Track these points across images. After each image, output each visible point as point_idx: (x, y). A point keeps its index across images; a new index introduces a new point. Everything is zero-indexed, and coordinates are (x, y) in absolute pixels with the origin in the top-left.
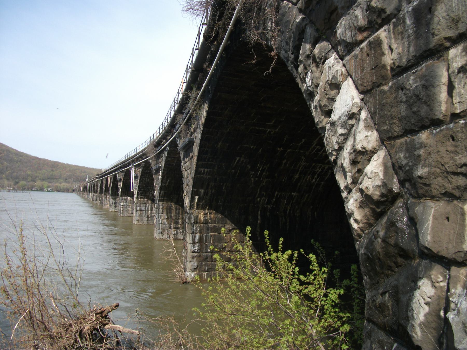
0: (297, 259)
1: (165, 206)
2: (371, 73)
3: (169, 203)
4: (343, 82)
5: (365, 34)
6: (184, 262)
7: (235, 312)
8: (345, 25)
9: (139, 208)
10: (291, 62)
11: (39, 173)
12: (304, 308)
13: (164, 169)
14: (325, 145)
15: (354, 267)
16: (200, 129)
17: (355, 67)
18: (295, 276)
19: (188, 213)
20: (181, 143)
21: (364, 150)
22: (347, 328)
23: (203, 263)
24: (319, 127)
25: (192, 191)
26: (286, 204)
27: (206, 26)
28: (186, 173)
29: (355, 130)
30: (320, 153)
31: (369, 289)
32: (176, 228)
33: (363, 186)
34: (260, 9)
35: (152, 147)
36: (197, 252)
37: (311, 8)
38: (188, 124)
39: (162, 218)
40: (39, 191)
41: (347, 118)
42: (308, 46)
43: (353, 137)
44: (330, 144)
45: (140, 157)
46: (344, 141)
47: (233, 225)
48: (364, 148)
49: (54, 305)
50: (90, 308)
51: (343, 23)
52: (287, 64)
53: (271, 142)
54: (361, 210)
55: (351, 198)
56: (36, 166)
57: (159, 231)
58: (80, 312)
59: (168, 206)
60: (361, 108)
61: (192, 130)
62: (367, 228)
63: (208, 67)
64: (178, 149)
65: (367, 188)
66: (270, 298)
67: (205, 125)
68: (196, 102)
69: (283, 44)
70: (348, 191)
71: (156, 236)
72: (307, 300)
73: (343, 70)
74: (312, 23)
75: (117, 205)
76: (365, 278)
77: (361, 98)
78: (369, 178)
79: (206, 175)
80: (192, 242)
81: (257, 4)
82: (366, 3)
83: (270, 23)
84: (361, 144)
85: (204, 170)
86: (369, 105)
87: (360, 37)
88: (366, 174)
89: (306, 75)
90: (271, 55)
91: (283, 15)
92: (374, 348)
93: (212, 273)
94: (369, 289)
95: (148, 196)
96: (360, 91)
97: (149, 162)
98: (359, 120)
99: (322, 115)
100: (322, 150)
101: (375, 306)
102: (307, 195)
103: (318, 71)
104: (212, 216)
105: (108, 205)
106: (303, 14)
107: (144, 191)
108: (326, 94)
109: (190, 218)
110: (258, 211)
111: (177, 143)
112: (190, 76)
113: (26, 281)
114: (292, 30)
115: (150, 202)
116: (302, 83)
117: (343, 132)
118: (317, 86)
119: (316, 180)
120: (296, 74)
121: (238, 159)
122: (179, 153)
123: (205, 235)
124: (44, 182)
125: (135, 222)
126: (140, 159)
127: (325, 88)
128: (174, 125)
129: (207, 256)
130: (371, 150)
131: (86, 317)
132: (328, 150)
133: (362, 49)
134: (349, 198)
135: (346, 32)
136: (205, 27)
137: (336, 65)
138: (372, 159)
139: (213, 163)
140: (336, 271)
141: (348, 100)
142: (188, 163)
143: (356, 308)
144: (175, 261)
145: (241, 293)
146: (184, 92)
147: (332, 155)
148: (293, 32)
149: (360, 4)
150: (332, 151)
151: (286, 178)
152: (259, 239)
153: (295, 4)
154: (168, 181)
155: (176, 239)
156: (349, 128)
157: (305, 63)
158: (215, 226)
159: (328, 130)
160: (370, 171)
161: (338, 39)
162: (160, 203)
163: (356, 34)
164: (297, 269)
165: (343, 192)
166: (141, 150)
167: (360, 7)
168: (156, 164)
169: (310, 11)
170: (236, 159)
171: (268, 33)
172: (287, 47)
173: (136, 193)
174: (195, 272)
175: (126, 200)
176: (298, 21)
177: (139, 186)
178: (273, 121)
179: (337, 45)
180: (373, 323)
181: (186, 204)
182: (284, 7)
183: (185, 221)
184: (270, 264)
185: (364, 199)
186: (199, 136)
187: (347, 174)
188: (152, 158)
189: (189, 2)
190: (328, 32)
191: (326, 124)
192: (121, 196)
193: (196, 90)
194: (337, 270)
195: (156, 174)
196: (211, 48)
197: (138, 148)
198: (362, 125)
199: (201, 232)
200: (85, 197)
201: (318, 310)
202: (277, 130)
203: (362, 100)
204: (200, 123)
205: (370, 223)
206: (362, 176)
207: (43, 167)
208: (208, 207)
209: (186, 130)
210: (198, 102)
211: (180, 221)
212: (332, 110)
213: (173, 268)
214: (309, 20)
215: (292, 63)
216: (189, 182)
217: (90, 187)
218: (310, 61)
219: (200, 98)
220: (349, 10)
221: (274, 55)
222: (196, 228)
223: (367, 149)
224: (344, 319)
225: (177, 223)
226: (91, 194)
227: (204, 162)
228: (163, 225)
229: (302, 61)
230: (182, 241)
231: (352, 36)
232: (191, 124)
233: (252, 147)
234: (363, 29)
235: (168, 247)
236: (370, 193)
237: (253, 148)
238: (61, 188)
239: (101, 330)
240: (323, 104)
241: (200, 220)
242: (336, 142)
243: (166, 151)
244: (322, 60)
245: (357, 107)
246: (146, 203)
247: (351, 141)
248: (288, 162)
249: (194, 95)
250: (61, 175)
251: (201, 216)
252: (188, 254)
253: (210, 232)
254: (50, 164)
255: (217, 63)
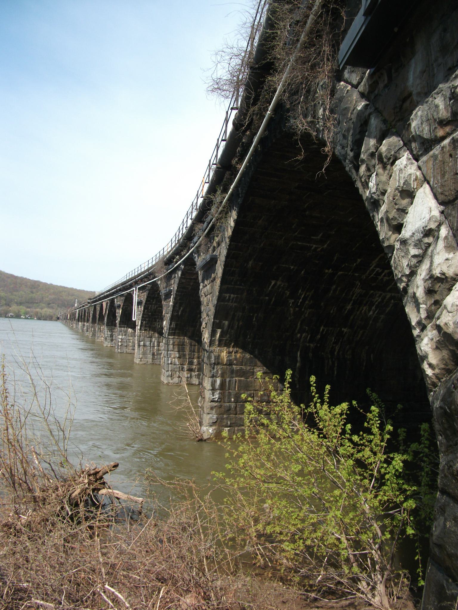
0: (348, 412)
1: (177, 341)
2: (454, 179)
3: (182, 338)
4: (417, 189)
5: (448, 129)
6: (200, 414)
7: (269, 479)
8: (421, 116)
9: (142, 342)
10: (350, 161)
11: (16, 295)
12: (357, 477)
13: (176, 294)
14: (393, 268)
15: (425, 426)
16: (226, 243)
17: (434, 170)
18: (346, 435)
19: (206, 351)
20: (199, 261)
21: (443, 277)
22: (411, 504)
23: (225, 416)
24: (385, 244)
25: (214, 322)
26: (334, 343)
27: (237, 111)
28: (205, 299)
29: (432, 251)
30: (380, 278)
31: (445, 452)
32: (190, 370)
33: (441, 322)
34: (308, 91)
35: (162, 264)
36: (217, 401)
37: (376, 92)
38: (210, 235)
39: (172, 357)
40: (15, 318)
41: (422, 235)
42: (372, 142)
43: (430, 259)
44: (399, 267)
45: (146, 277)
46: (418, 264)
47: (265, 368)
48: (444, 274)
49: (37, 463)
50: (81, 467)
51: (419, 113)
52: (344, 164)
53: (317, 262)
54: (437, 352)
55: (424, 337)
56: (12, 286)
57: (168, 373)
58: (66, 471)
59: (180, 342)
60: (440, 223)
61: (215, 244)
62: (444, 375)
63: (237, 163)
64: (195, 268)
65: (446, 324)
66: (313, 462)
67: (233, 238)
68: (221, 208)
69: (340, 137)
70: (421, 327)
71: (164, 379)
72: (359, 467)
73: (419, 173)
74: (379, 112)
75: (114, 338)
76: (440, 437)
77: (440, 210)
78: (449, 312)
79: (232, 302)
80: (211, 388)
81: (306, 85)
82: (449, 90)
83: (322, 109)
84: (440, 269)
85: (230, 297)
86: (450, 220)
87: (440, 133)
88: (445, 307)
89: (369, 179)
90: (324, 151)
91: (341, 100)
92: (448, 526)
93: (236, 429)
94: (444, 452)
95: (155, 328)
96: (440, 202)
97: (157, 284)
98: (438, 238)
99: (390, 230)
100: (383, 274)
101: (452, 474)
102: (361, 332)
103: (386, 174)
104: (238, 355)
105: (103, 338)
106: (366, 100)
107: (149, 321)
108: (396, 204)
109: (209, 358)
110: (298, 351)
111: (194, 260)
112: (214, 174)
113: (7, 430)
114: (351, 119)
115: (156, 335)
116: (364, 188)
117: (417, 253)
118: (384, 193)
119: (374, 313)
120: (356, 177)
121: (273, 283)
122: (197, 273)
123: (228, 380)
124: (21, 307)
125: (137, 361)
126: (146, 280)
127: (394, 196)
128: (192, 237)
129: (230, 406)
130: (452, 277)
131: (76, 479)
132: (396, 275)
133: (443, 148)
134: (422, 336)
135: (423, 126)
136: (235, 112)
137: (409, 168)
138: (454, 288)
139: (241, 287)
140: (401, 431)
141: (424, 213)
142: (208, 287)
143: (424, 480)
144: (189, 412)
145: (276, 455)
146: (206, 194)
147: (402, 281)
148: (353, 122)
149: (442, 90)
150: (402, 276)
151: (335, 309)
152: (298, 387)
153: (356, 86)
154: (182, 308)
155: (189, 384)
156: (424, 249)
157: (369, 162)
158: (241, 369)
159: (397, 250)
160: (451, 303)
161: (412, 133)
162: (170, 337)
163: (436, 128)
164: (349, 426)
165: (415, 329)
166: (146, 268)
167: (441, 94)
168: (166, 287)
169: (375, 97)
170: (271, 283)
171: (318, 122)
172: (345, 141)
173: (139, 323)
174: (214, 427)
175: (126, 332)
176: (359, 108)
177: (143, 314)
178: (321, 235)
179: (410, 141)
180: (449, 495)
181: (205, 340)
182: (342, 90)
183: (203, 360)
184: (317, 419)
185: (442, 338)
186: (224, 252)
187: (421, 306)
188: (161, 279)
189: (216, 80)
190: (398, 124)
191: (394, 242)
192: (120, 327)
193: (222, 192)
194: (403, 429)
195: (165, 299)
196: (242, 139)
197: (142, 266)
198: (441, 244)
199: (222, 376)
200: (73, 327)
201: (374, 480)
202: (325, 246)
203: (442, 212)
204: (226, 235)
205: (449, 369)
206: (440, 309)
207: (20, 287)
208: (233, 344)
209: (207, 244)
210: (224, 208)
211: (195, 361)
212: (403, 224)
213: (186, 420)
214: (373, 108)
215: (351, 162)
216: (210, 310)
217: (79, 314)
218: (375, 161)
219: (227, 203)
220: (427, 97)
221: (328, 151)
222: (217, 371)
223: (447, 275)
224: (408, 493)
225: (191, 363)
226: (80, 323)
227: (229, 286)
228: (173, 366)
229: (364, 160)
230: (197, 387)
231: (430, 131)
232: (214, 237)
233: (292, 267)
234: (444, 123)
235: (179, 394)
236: (450, 330)
237: (294, 269)
238: (43, 315)
239: (94, 496)
240: (391, 216)
241: (223, 360)
242: (408, 265)
243: (179, 270)
244: (391, 161)
245: (435, 221)
246: (151, 337)
247: (426, 265)
248: (339, 288)
249: (218, 199)
250: (43, 298)
251: (224, 354)
252: (206, 403)
253: (234, 375)
254: (29, 284)
255: (249, 159)
